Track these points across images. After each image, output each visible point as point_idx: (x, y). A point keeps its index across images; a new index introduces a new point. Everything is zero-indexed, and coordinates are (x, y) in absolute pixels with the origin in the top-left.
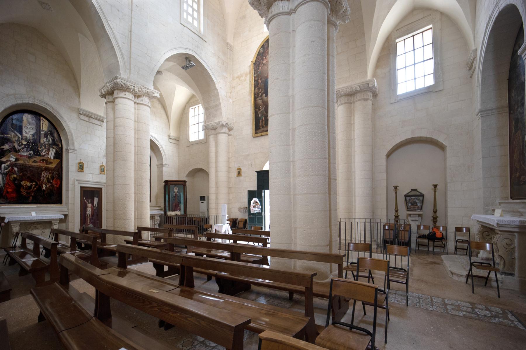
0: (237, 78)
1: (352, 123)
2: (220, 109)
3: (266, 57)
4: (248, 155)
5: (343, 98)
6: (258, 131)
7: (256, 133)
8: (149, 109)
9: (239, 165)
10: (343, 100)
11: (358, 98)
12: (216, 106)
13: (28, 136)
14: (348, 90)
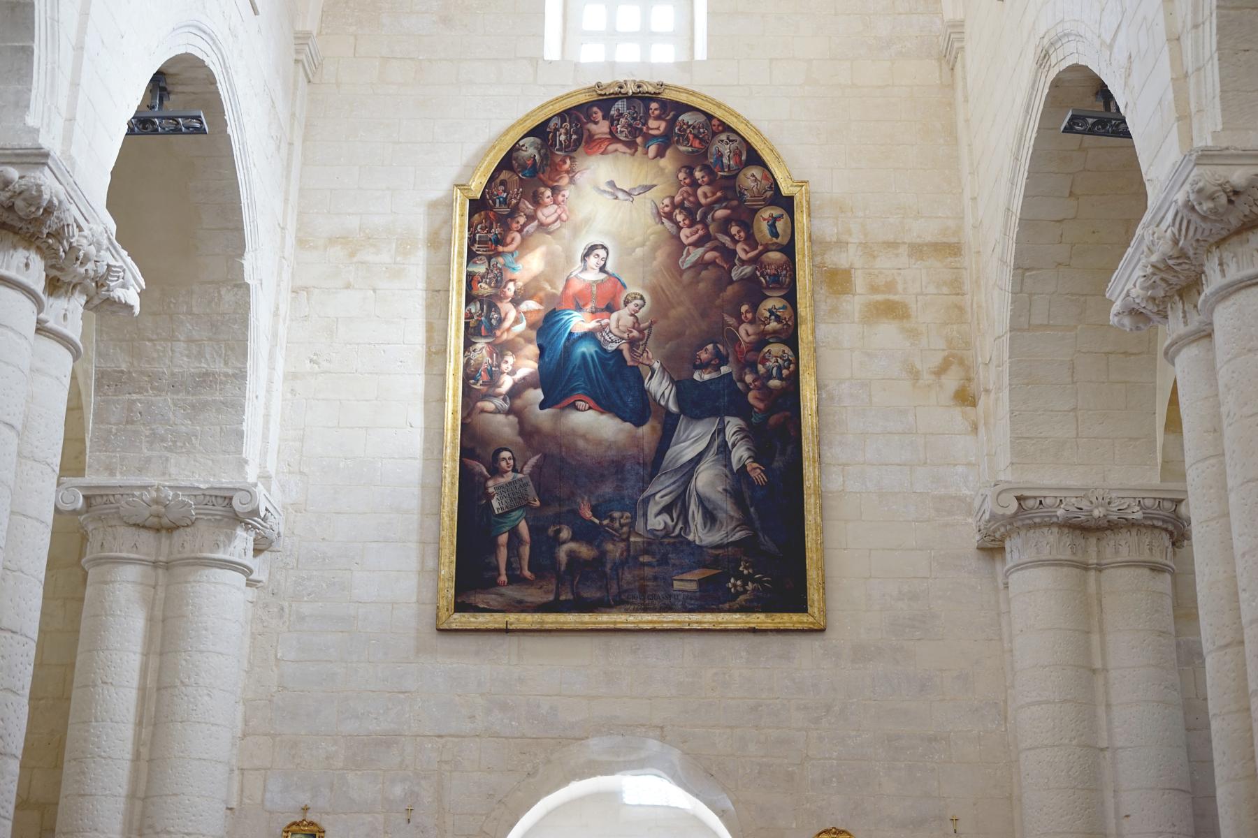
0: (332, 241)
1: (1098, 664)
2: (237, 407)
3: (555, 190)
4: (388, 741)
5: (1052, 536)
6: (479, 599)
7: (461, 606)
8: (68, 358)
9: (305, 798)
10: (1051, 543)
11: (1124, 555)
12: (205, 380)
13: (244, 534)
14: (1084, 504)
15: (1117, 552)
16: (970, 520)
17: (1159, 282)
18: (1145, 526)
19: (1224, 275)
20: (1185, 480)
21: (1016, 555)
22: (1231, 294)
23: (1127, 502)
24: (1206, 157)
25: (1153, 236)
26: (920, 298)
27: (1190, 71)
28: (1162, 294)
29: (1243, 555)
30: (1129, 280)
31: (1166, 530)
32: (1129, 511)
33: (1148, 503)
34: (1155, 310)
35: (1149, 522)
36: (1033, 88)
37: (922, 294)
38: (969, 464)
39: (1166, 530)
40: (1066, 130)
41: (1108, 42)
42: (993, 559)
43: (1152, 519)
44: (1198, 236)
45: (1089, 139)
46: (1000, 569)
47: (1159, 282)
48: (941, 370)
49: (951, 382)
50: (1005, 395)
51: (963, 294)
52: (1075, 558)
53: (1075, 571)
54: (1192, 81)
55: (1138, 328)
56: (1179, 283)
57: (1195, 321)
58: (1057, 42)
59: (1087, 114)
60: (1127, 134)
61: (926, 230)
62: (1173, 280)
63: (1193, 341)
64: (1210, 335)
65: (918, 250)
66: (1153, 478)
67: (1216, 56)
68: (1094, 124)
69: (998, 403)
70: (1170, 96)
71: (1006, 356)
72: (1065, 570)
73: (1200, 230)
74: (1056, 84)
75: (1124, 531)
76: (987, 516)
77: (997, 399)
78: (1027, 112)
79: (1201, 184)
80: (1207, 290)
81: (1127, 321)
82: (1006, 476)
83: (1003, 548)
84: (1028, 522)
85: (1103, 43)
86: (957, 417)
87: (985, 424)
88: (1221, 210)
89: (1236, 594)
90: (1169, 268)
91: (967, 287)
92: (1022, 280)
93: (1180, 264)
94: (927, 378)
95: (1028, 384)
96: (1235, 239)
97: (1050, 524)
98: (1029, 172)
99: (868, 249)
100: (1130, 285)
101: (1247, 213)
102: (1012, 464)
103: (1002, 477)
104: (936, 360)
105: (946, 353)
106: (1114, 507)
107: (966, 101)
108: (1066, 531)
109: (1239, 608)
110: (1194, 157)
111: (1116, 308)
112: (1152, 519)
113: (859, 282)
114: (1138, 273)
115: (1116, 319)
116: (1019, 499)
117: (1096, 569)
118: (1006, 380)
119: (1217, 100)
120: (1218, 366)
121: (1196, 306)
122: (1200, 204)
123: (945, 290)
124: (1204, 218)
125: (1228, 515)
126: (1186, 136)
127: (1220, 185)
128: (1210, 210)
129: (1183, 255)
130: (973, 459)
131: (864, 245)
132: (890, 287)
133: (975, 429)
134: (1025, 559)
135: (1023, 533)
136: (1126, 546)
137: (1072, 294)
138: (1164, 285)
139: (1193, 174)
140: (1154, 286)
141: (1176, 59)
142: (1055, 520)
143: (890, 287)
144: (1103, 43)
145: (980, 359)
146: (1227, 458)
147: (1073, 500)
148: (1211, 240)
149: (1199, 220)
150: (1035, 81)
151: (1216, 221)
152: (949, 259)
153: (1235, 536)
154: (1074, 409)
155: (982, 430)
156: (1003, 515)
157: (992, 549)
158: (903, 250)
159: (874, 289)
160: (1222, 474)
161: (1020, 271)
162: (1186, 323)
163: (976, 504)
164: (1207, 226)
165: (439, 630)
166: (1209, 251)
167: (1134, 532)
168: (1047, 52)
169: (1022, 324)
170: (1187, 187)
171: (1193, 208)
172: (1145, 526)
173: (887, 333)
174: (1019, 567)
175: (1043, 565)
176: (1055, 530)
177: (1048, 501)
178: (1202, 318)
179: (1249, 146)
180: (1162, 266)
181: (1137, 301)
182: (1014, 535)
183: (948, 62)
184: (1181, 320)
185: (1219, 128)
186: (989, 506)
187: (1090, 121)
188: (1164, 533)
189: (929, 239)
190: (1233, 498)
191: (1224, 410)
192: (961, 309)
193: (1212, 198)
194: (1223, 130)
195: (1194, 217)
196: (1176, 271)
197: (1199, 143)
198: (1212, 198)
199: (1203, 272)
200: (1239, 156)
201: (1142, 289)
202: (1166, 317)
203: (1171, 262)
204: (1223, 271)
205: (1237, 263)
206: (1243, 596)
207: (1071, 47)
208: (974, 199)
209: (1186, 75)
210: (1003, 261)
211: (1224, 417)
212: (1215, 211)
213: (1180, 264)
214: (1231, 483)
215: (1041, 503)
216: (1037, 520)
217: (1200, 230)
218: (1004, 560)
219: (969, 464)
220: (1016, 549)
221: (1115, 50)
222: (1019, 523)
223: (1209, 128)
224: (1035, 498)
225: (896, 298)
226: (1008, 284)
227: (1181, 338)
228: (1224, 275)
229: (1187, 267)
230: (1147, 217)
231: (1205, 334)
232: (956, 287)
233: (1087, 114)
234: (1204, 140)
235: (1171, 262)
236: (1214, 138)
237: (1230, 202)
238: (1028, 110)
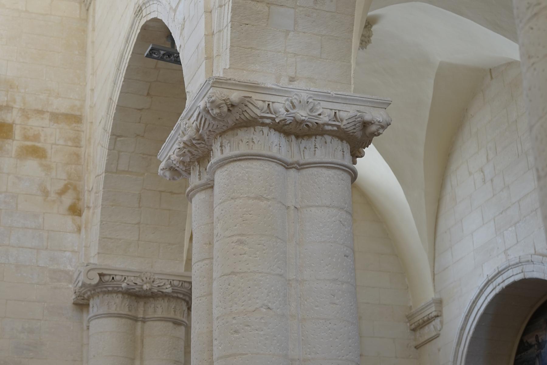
10: (117, 303)
14: (139, 281)
15: (155, 311)
16: (70, 286)
17: (187, 153)
18: (173, 297)
19: (222, 153)
20: (191, 271)
21: (95, 309)
22: (225, 164)
23: (164, 281)
24: (217, 83)
25: (186, 125)
26: (53, 146)
27: (215, 32)
28: (188, 160)
29: (218, 318)
30: (171, 151)
31: (185, 300)
32: (164, 287)
33: (176, 283)
34: (184, 169)
35: (175, 295)
36: (131, 28)
37: (55, 144)
38: (73, 251)
39: (185, 300)
40: (147, 56)
41: (174, 7)
42: (82, 310)
43: (177, 293)
44: (210, 128)
45: (161, 63)
46: (85, 317)
47: (187, 153)
48: (62, 192)
49: (68, 200)
50: (99, 210)
51: (80, 147)
52: (130, 313)
53: (130, 321)
54: (216, 37)
55: (174, 179)
56: (197, 154)
57: (205, 177)
58: (147, 3)
59: (158, 48)
60: (179, 63)
61: (61, 105)
62: (195, 153)
63: (202, 190)
64: (212, 187)
65: (55, 117)
66: (180, 269)
67: (230, 25)
68: (164, 55)
69: (94, 216)
70: (203, 44)
71: (102, 187)
72: (124, 320)
73: (211, 125)
74: (145, 28)
75: (160, 299)
76: (80, 284)
77: (94, 213)
78: (127, 42)
79: (213, 98)
80: (213, 161)
81: (168, 174)
82: (95, 260)
83: (88, 305)
84: (104, 289)
85: (171, 8)
86: (69, 221)
87: (85, 227)
88: (223, 115)
89: (212, 341)
90: (193, 145)
91: (83, 143)
92: (115, 142)
93: (199, 143)
94: (53, 196)
95: (112, 206)
96: (230, 133)
97: (116, 291)
98: (125, 78)
99: (25, 113)
100: (171, 153)
101: (238, 118)
102: (99, 253)
103: (92, 261)
104: (60, 185)
105: (66, 182)
106: (156, 284)
107: (94, 30)
108: (127, 296)
109: (212, 350)
110: (211, 82)
111: (162, 165)
112: (177, 293)
113: (18, 132)
114: (176, 146)
115: (162, 172)
116: (101, 275)
117: (141, 321)
118: (100, 202)
119: (228, 50)
120: (215, 206)
121: (206, 169)
122: (212, 110)
123: (70, 143)
124: (214, 118)
125: (211, 294)
126: (210, 69)
127: (224, 100)
128: (218, 114)
129: (201, 138)
130: (76, 248)
131: (23, 110)
132: (36, 137)
133: (79, 230)
134: (101, 312)
135: (101, 296)
136: (161, 308)
137: (144, 154)
138: (190, 155)
139: (210, 92)
140: (184, 155)
141: (209, 24)
142: (120, 289)
143: (36, 137)
144: (171, 8)
145: (86, 188)
146: (214, 260)
147: (132, 278)
148: (217, 132)
149: (211, 119)
150: (132, 25)
151: (220, 121)
152: (74, 125)
153: (214, 307)
154: (139, 223)
155: (83, 230)
156: (90, 284)
157: (82, 304)
158: (47, 116)
159: (26, 138)
160: (211, 270)
161: (114, 137)
162: (200, 179)
163: (75, 276)
164: (216, 123)
165: (490, 69)
166: (216, 138)
167: (166, 300)
168: (141, 8)
169: (112, 169)
170: (206, 99)
171: (208, 112)
172: (173, 297)
173: (31, 166)
174: (97, 317)
175: (111, 317)
176: (120, 295)
177: (117, 278)
178: (208, 176)
179: (242, 80)
180: (189, 143)
181: (174, 162)
182: (96, 297)
183: (85, 5)
184: (198, 177)
185: (228, 67)
186: (82, 278)
187: (162, 52)
188: (183, 302)
189: (63, 111)
190: (215, 284)
191: (215, 232)
192: (78, 156)
193: (219, 107)
194: (230, 68)
195: (209, 117)
196: (197, 148)
197: (216, 74)
198: (219, 107)
199: (212, 150)
200: (236, 85)
201: (177, 156)
202: (190, 174)
203: (194, 142)
204: (222, 150)
205: (230, 146)
206: (215, 343)
207: (154, 7)
208: (92, 90)
209: (213, 34)
210: (105, 130)
211: (215, 237)
212: (220, 115)
213: (199, 143)
214: (215, 275)
215: (113, 278)
216: (110, 289)
217: (211, 125)
218: (88, 311)
219: (73, 251)
220: (97, 306)
221: (177, 13)
222: (99, 290)
223: (222, 67)
224: (110, 275)
225: (39, 145)
226: (106, 145)
227: (196, 187)
228: (222, 153)
229: (203, 145)
230: (184, 113)
231: (209, 186)
232: (76, 141)
233: (158, 48)
234: (219, 73)
235: (194, 142)
236: (224, 73)
237: (229, 110)
238: (127, 40)
